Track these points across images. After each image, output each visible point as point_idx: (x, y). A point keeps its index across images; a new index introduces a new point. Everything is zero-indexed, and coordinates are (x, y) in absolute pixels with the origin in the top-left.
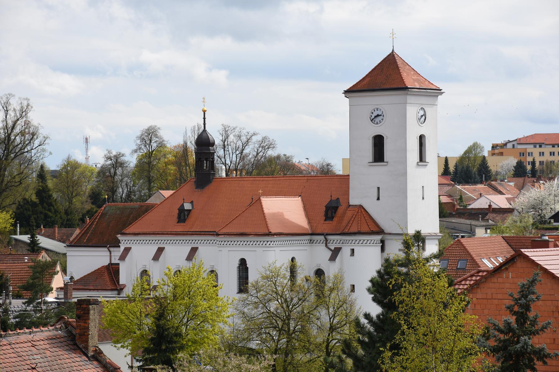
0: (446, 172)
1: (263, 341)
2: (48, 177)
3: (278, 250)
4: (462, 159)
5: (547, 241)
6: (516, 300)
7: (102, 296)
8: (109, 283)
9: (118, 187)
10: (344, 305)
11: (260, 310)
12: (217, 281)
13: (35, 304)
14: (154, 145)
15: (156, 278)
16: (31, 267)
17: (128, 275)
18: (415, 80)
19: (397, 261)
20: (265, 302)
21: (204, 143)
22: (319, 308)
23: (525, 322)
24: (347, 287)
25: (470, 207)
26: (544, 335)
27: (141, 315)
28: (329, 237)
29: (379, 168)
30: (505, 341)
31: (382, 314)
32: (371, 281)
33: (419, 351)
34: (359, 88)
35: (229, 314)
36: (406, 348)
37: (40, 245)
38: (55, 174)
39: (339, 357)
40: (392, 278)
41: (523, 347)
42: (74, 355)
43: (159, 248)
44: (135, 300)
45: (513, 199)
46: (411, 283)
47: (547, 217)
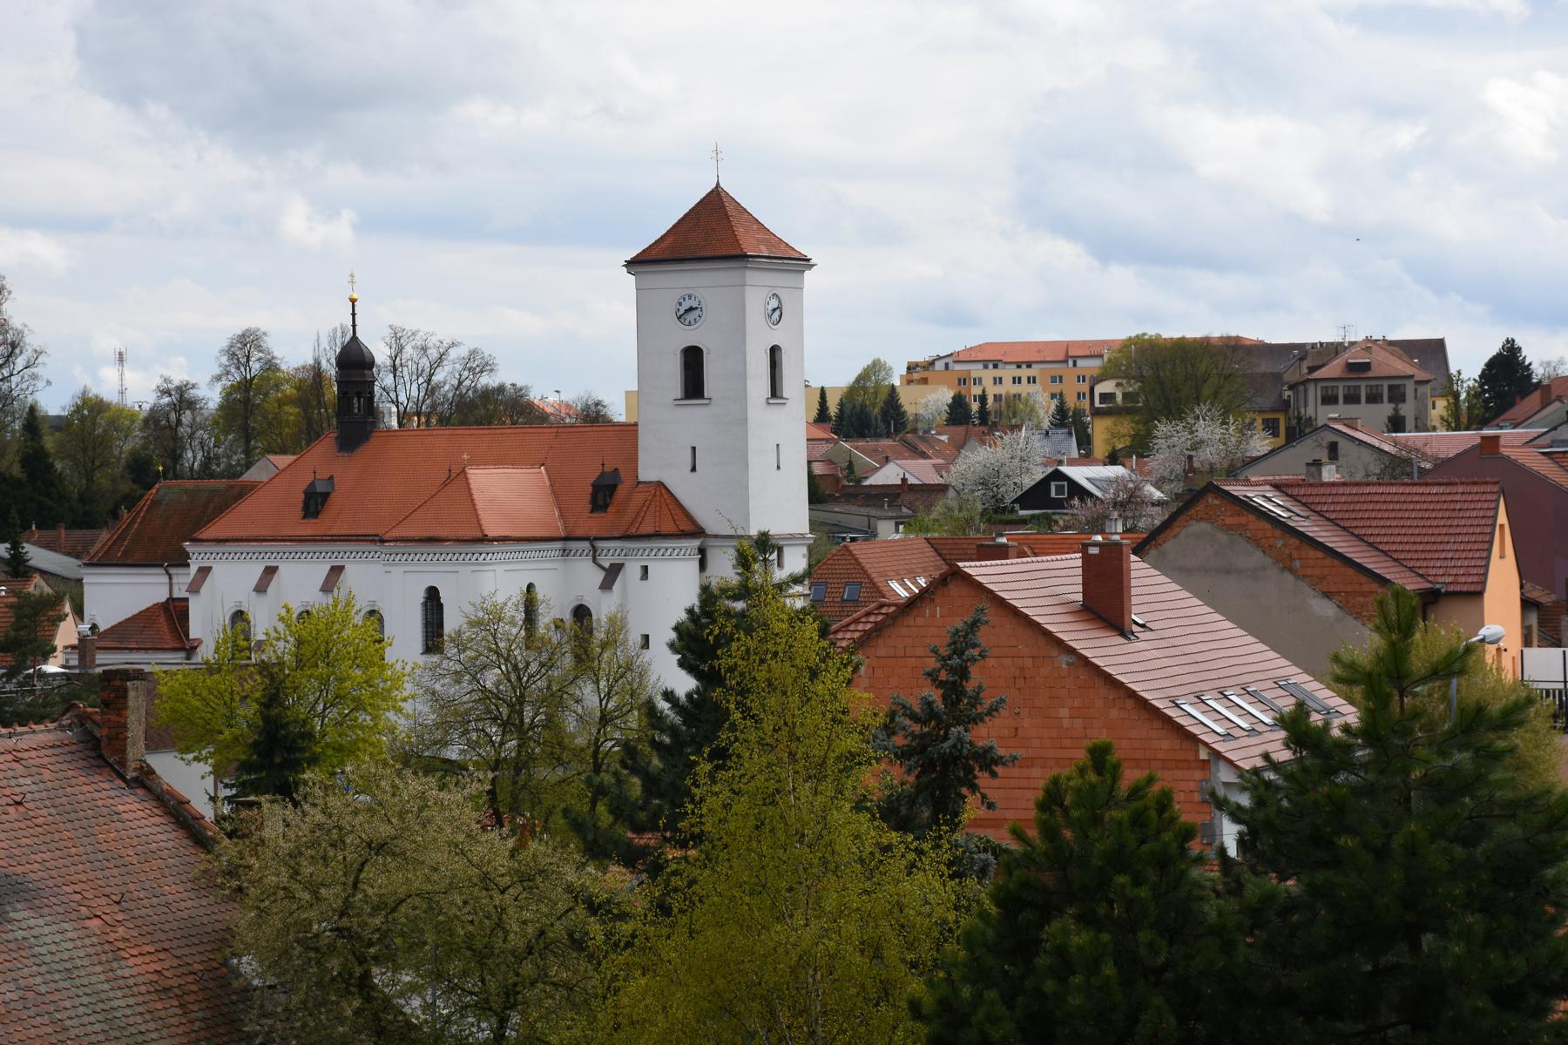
0: (822, 416)
1: (473, 745)
2: (45, 429)
3: (500, 569)
4: (852, 391)
5: (1005, 546)
6: (943, 659)
7: (150, 662)
8: (168, 637)
9: (184, 448)
10: (628, 675)
11: (466, 686)
12: (382, 631)
13: (21, 678)
14: (256, 366)
15: (263, 623)
16: (11, 606)
17: (206, 623)
18: (760, 241)
19: (723, 591)
20: (474, 671)
21: (354, 361)
22: (579, 682)
23: (959, 700)
24: (634, 638)
25: (867, 483)
26: (998, 721)
27: (232, 700)
28: (601, 544)
29: (694, 412)
30: (923, 736)
31: (697, 691)
32: (676, 629)
33: (764, 760)
34: (653, 255)
35: (405, 694)
36: (739, 756)
37: (31, 563)
38: (60, 424)
39: (616, 774)
40: (714, 622)
41: (954, 746)
42: (98, 778)
43: (267, 568)
44: (219, 670)
45: (946, 467)
46: (749, 631)
47: (1008, 501)
